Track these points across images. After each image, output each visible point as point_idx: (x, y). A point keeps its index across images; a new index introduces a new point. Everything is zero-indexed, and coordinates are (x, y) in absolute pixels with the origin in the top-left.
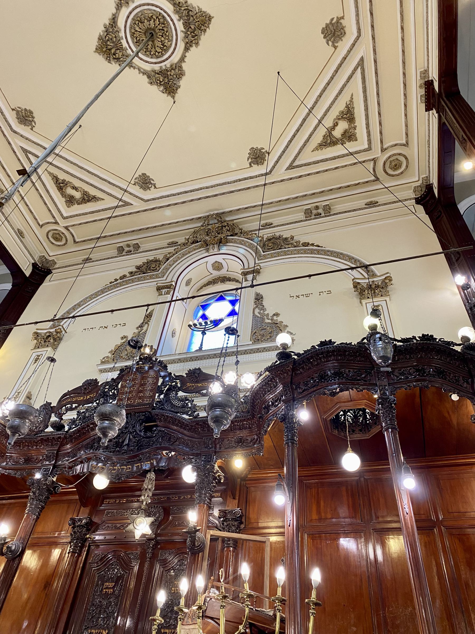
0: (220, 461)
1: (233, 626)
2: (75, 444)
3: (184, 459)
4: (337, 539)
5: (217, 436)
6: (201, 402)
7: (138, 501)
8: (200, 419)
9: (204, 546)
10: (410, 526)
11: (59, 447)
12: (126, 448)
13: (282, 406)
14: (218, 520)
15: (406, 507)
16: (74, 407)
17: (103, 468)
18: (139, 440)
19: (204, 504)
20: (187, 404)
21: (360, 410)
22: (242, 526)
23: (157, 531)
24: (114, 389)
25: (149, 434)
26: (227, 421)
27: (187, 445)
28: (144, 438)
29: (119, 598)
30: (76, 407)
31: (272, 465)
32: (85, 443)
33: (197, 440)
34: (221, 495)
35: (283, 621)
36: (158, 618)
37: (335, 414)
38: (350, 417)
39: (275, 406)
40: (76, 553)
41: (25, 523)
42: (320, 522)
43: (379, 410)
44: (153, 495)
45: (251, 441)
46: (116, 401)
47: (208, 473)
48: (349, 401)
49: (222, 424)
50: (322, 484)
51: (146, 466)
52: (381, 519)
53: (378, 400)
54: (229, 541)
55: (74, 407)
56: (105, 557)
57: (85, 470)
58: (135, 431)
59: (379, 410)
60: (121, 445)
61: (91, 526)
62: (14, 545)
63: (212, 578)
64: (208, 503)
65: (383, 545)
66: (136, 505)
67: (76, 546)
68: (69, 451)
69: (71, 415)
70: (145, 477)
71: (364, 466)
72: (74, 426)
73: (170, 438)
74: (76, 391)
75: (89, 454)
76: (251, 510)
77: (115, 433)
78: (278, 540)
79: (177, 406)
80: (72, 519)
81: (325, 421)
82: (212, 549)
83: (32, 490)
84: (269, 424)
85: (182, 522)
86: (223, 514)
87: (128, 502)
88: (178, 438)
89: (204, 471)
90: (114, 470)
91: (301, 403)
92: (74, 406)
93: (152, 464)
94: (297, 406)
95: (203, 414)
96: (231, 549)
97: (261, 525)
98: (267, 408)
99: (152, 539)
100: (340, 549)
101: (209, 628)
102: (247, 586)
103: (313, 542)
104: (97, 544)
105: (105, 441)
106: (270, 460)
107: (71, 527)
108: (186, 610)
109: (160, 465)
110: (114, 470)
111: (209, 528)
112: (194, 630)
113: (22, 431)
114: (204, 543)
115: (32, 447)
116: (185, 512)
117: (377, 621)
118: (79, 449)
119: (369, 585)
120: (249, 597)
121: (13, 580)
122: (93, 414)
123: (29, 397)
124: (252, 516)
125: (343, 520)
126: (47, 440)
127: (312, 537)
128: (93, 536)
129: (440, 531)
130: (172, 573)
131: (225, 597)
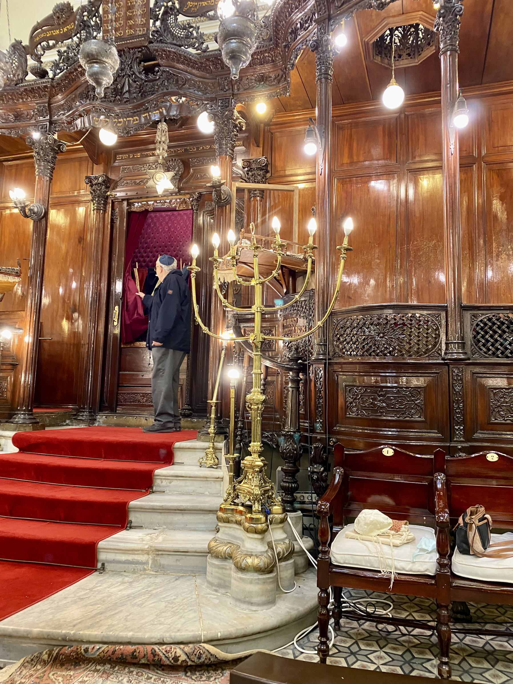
0: (239, 104)
3: (197, 105)
4: (368, 182)
6: (208, 28)
7: (153, 155)
8: (211, 53)
10: (453, 168)
11: (50, 99)
12: (127, 95)
13: (313, 28)
15: (451, 147)
18: (141, 85)
19: (226, 155)
20: (192, 33)
21: (412, 26)
22: (269, 175)
24: (95, 16)
25: (151, 76)
26: (246, 56)
28: (146, 81)
32: (78, 92)
34: (243, 143)
35: (313, 263)
36: (195, 268)
37: (380, 35)
38: (398, 37)
39: (306, 29)
40: (100, 210)
41: (39, 185)
42: (351, 166)
43: (438, 25)
44: (169, 147)
45: (275, 78)
46: (101, 33)
47: (228, 121)
48: (399, 15)
49: (241, 61)
50: (356, 125)
51: (155, 116)
53: (440, 11)
54: (256, 190)
57: (87, 125)
58: (134, 73)
59: (439, 24)
60: (121, 93)
62: (36, 206)
63: (242, 230)
65: (416, 184)
66: (152, 159)
68: (62, 102)
69: (50, 57)
70: (157, 128)
71: (410, 100)
73: (177, 81)
74: (48, 22)
75: (86, 105)
76: (277, 159)
77: (109, 79)
78: (307, 187)
79: (179, 37)
80: (87, 177)
81: (366, 45)
83: (35, 150)
84: (297, 55)
86: (248, 164)
87: (143, 156)
88: (187, 80)
89: (223, 119)
90: (120, 122)
91: (339, 23)
92: (51, 43)
94: (333, 27)
95: (213, 46)
96: (258, 198)
97: (287, 173)
98: (295, 32)
100: (371, 191)
101: (243, 270)
103: (343, 186)
105: (100, 91)
106: (297, 100)
107: (88, 185)
109: (171, 114)
110: (120, 122)
111: (233, 179)
115: (18, 100)
118: (73, 100)
121: (45, 239)
124: (279, 164)
125: (376, 162)
126: (32, 91)
127: (342, 181)
128: (113, 193)
129: (480, 168)
131: (257, 248)
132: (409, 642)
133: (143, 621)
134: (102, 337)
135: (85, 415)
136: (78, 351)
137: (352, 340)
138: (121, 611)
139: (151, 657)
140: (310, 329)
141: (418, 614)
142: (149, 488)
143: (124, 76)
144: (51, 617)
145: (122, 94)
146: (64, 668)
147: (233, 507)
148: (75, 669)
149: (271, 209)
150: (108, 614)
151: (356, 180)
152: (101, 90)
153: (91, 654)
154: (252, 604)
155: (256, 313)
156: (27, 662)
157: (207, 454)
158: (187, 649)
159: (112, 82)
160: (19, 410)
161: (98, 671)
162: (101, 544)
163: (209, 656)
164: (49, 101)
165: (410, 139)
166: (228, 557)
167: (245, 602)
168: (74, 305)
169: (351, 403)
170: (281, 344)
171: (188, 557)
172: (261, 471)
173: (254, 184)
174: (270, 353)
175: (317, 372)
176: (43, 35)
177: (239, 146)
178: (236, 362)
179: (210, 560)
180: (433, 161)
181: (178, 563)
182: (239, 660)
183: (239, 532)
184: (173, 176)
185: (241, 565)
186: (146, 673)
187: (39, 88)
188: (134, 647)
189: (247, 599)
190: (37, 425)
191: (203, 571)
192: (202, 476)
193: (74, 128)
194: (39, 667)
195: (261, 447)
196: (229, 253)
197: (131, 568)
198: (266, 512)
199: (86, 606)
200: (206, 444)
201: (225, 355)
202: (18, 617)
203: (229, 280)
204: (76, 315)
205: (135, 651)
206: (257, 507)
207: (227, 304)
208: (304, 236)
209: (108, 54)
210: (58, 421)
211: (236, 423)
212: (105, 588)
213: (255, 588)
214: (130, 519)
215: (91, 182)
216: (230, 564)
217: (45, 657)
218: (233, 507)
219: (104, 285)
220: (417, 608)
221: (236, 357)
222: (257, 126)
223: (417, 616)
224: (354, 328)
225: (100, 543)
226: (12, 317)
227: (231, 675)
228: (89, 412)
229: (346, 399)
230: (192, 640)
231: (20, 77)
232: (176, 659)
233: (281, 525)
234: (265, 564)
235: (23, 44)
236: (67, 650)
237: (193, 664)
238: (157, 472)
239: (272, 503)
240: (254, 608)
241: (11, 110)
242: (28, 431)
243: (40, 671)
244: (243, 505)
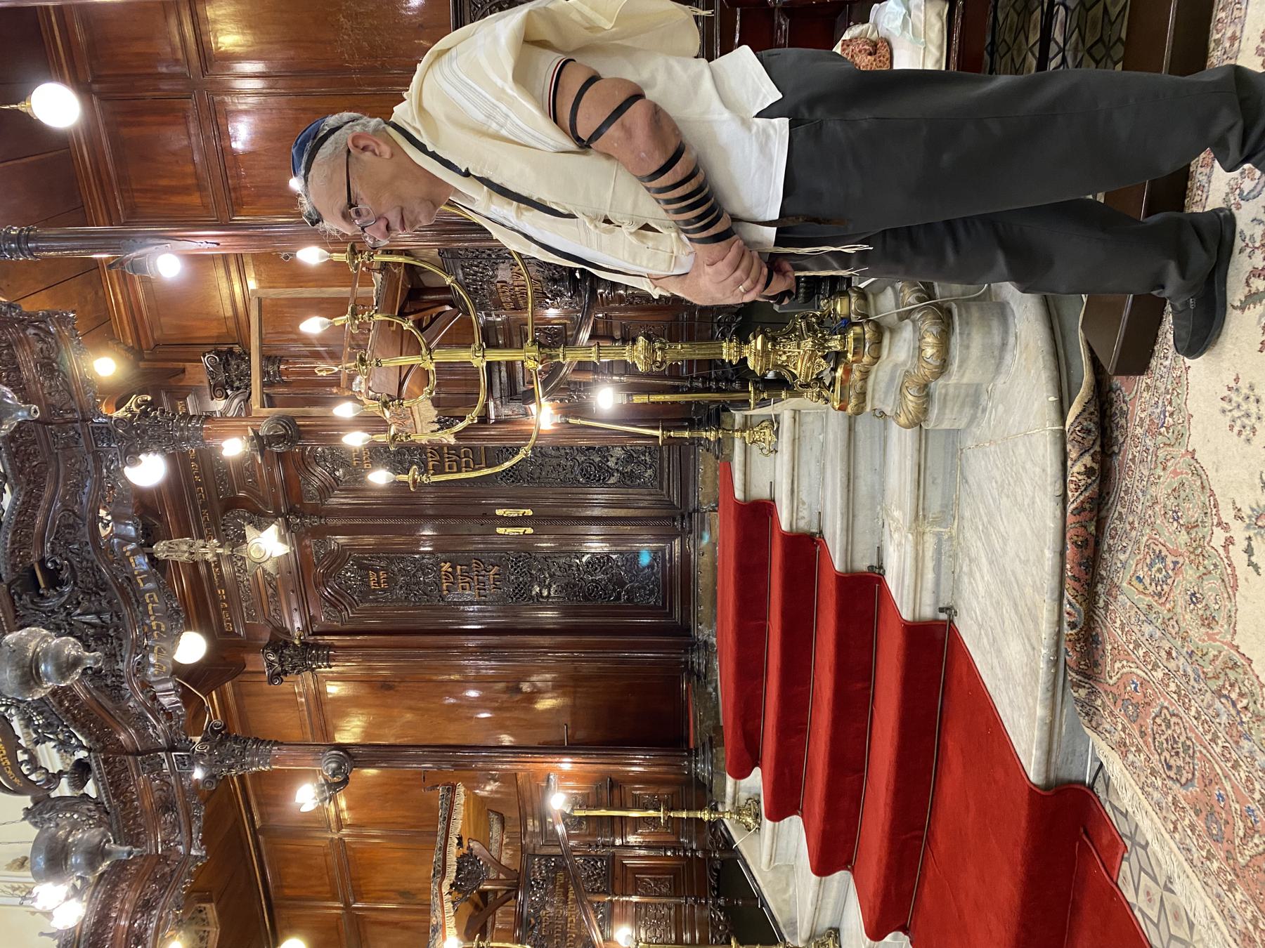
0: (104, 409)
2: (114, 725)
3: (112, 488)
4: (234, 153)
5: (35, 412)
7: (218, 565)
8: (7, 466)
11: (128, 753)
12: (106, 617)
16: (26, 757)
17: (159, 651)
18: (83, 592)
19: (202, 429)
22: (237, 349)
23: (270, 516)
25: (65, 575)
27: (79, 486)
28: (75, 583)
29: (392, 556)
30: (26, 751)
31: (96, 293)
32: (108, 704)
33: (61, 465)
36: (412, 475)
42: (205, 189)
44: (201, 537)
45: (43, 341)
52: (180, 55)
54: (268, 373)
55: (26, 757)
56: (328, 601)
57: (170, 685)
58: (63, 605)
60: (102, 627)
61: (280, 642)
66: (226, 568)
67: (317, 658)
68: (132, 731)
69: (51, 758)
70: (166, 561)
72: (73, 741)
77: (67, 643)
80: (271, 681)
82: (288, 403)
86: (219, 389)
88: (66, 508)
89: (135, 439)
90: (159, 626)
92: (22, 757)
93: (134, 553)
97: (229, 313)
99: (287, 520)
102: (339, 321)
103: (247, 204)
104: (309, 621)
105: (92, 659)
108: (393, 430)
109: (133, 534)
110: (159, 626)
113: (97, 840)
114: (279, 419)
115: (136, 808)
116: (226, 464)
117: (369, 85)
118: (126, 712)
119: (310, 94)
122: (29, 703)
123: (22, 863)
124: (213, 331)
125: (193, 139)
126: (116, 785)
127: (237, 205)
128: (297, 633)
131: (362, 361)
132: (1076, 50)
133: (1029, 532)
134: (559, 639)
135: (697, 659)
136: (587, 678)
138: (1013, 572)
139: (1086, 515)
141: (1031, 35)
142: (814, 540)
143: (70, 624)
144: (1019, 689)
145: (104, 626)
146: (1100, 661)
147: (838, 386)
148: (1103, 643)
150: (1017, 593)
152: (88, 658)
153: (1080, 619)
154: (1004, 345)
155: (489, 358)
156: (1090, 721)
157: (754, 442)
158: (1073, 455)
159: (72, 639)
160: (690, 772)
161: (1107, 604)
162: (907, 615)
163: (1086, 415)
164: (131, 754)
165: (141, 71)
166: (925, 392)
167: (1001, 358)
168: (508, 690)
171: (929, 464)
172: (774, 340)
176: (10, 772)
177: (186, 406)
179: (930, 425)
180: (180, 24)
181: (939, 481)
182: (1094, 361)
183: (880, 374)
185: (936, 367)
186: (1113, 523)
187: (108, 773)
188: (1068, 541)
189: (996, 353)
190: (714, 741)
191: (953, 435)
192: (790, 448)
193: (179, 708)
194: (1099, 702)
195: (731, 341)
197: (948, 559)
198: (847, 323)
199: (1004, 632)
200: (738, 445)
201: (577, 418)
202: (1019, 743)
204: (526, 687)
205: (1075, 543)
206: (835, 344)
208: (334, 272)
209: (20, 647)
210: (710, 705)
211: (698, 391)
212: (978, 603)
213: (977, 341)
214: (865, 569)
215: (279, 674)
216: (938, 387)
217: (1083, 693)
218: (838, 386)
219: (472, 642)
220: (1022, 36)
221: (579, 397)
222: (144, 374)
223: (1035, 37)
225: (904, 617)
226: (527, 794)
227: (1117, 373)
228: (693, 651)
230: (1059, 447)
231: (92, 807)
232: (1089, 472)
233: (871, 297)
234: (935, 324)
235: (30, 805)
236: (1072, 658)
237: (1098, 443)
238: (785, 526)
239: (831, 315)
240: (1012, 340)
241: (156, 819)
242: (724, 754)
243: (1106, 699)
244: (834, 369)
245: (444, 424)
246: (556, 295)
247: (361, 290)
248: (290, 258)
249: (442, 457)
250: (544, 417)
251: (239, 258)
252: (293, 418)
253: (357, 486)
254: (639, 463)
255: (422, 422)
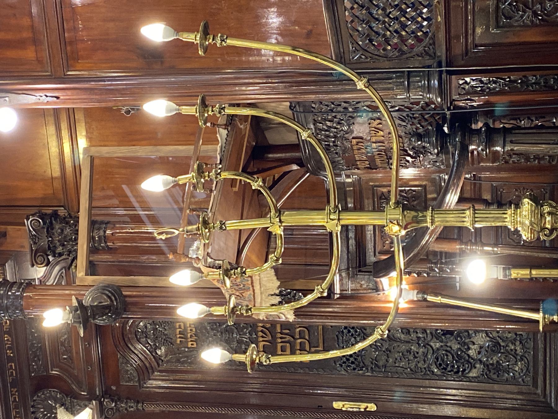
1: (249, 210)
9: (108, 286)
14: (53, 268)
19: (22, 297)
22: (62, 212)
36: (250, 355)
54: (93, 238)
64: (19, 288)
78: (84, 133)
85: (63, 344)
86: (40, 255)
96: (108, 232)
97: (57, 173)
99: (101, 404)
101: (254, 258)
102: (183, 179)
112: (263, 283)
114: (105, 288)
120: (203, 172)
124: (39, 191)
127: (71, 59)
130: (161, 352)
131: (205, 223)
137: (396, 18)
140: (375, 109)
149: (127, 205)
151: (69, 31)
155: (343, 222)
169: (535, 14)
170: (408, 173)
173: (80, 242)
174: (429, 196)
175: (469, 89)
178: (452, 270)
184: (67, 409)
196: (219, 285)
201: (436, 295)
203: (273, 284)
207: (325, 285)
221: (441, 270)
224: (371, 14)
229: (525, 26)
245: (286, 297)
246: (418, 152)
247: (205, 149)
248: (135, 113)
249: (274, 337)
250: (396, 293)
251: (71, 113)
252: (119, 287)
253: (186, 367)
254: (507, 353)
255: (263, 295)
